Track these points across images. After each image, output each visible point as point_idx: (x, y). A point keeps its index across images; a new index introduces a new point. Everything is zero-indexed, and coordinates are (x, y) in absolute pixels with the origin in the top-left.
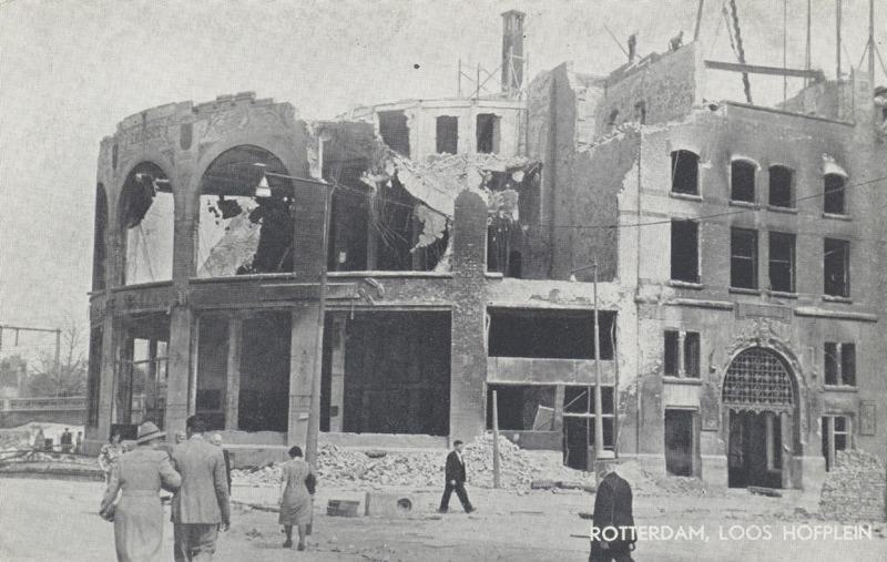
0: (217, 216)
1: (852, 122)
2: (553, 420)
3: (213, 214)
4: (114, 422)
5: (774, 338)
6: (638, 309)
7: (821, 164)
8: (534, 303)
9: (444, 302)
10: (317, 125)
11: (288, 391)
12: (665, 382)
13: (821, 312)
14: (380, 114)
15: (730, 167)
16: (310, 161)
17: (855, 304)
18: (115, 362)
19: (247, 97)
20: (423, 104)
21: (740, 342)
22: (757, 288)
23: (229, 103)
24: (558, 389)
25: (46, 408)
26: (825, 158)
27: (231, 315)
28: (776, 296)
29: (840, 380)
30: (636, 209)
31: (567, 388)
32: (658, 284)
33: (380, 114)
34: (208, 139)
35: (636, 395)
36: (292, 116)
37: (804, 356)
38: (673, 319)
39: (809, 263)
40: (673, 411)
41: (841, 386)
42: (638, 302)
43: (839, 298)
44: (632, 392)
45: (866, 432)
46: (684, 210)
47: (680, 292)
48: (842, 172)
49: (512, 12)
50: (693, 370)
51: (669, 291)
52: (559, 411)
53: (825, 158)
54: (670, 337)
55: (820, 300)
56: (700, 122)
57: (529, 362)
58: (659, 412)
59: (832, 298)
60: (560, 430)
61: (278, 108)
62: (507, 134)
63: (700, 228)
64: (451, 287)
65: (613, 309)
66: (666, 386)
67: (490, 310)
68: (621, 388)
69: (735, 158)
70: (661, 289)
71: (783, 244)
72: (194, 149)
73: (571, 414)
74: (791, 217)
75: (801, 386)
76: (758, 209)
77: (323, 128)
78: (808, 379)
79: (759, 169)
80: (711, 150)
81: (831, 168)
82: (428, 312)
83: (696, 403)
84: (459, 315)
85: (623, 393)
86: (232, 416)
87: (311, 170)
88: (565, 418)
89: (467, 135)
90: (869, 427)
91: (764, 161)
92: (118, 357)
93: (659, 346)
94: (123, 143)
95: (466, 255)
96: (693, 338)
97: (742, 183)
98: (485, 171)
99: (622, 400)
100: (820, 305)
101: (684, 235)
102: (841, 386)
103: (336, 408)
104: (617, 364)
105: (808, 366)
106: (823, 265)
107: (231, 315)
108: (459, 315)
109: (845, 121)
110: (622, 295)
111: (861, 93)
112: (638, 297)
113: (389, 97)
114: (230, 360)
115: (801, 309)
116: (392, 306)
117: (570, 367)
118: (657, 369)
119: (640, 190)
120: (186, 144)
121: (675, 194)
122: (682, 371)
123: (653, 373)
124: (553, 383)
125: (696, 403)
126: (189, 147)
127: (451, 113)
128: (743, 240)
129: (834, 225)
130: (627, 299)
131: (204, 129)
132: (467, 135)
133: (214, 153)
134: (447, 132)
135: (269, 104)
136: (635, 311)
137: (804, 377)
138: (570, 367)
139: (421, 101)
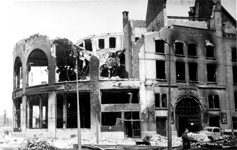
0: (47, 72)
1: (214, 30)
2: (121, 122)
3: (46, 71)
4: (15, 127)
5: (192, 95)
6: (146, 88)
7: (205, 43)
8: (114, 87)
9: (88, 89)
10: (53, 41)
12: (156, 110)
13: (207, 87)
14: (84, 40)
15: (175, 44)
16: (51, 51)
17: (218, 84)
19: (37, 35)
20: (95, 36)
21: (180, 97)
22: (185, 80)
23: (32, 38)
24: (122, 113)
26: (206, 41)
27: (39, 97)
28: (192, 83)
29: (214, 107)
30: (144, 58)
31: (125, 113)
32: (152, 80)
33: (84, 40)
35: (146, 113)
36: (47, 39)
37: (202, 100)
38: (158, 90)
39: (202, 72)
40: (158, 118)
41: (214, 109)
42: (146, 86)
43: (213, 82)
44: (145, 113)
45: (226, 122)
46: (160, 57)
47: (160, 82)
48: (212, 45)
49: (125, 12)
50: (164, 105)
51: (155, 82)
52: (123, 119)
53: (206, 41)
54: (157, 96)
55: (207, 83)
56: (164, 31)
57: (113, 105)
58: (154, 118)
59: (210, 82)
60: (123, 125)
61: (43, 37)
62: (118, 42)
63: (166, 63)
64: (90, 84)
65: (138, 88)
66: (156, 111)
67: (101, 90)
68: (141, 112)
69: (176, 42)
70: (153, 81)
71: (194, 67)
72: (26, 51)
74: (196, 59)
75: (201, 109)
76: (185, 57)
77: (55, 42)
78: (204, 107)
79: (184, 45)
81: (208, 44)
82: (84, 92)
83: (166, 115)
84: (92, 92)
85: (142, 113)
87: (52, 54)
88: (125, 122)
89: (107, 44)
90: (225, 121)
91: (186, 42)
93: (153, 98)
95: (94, 75)
96: (164, 96)
97: (179, 49)
98: (110, 53)
99: (142, 115)
100: (206, 85)
101: (160, 65)
102: (214, 109)
103: (64, 121)
104: (140, 104)
105: (203, 102)
106: (207, 73)
107: (39, 97)
108: (92, 92)
109: (212, 30)
110: (140, 84)
111: (217, 21)
112: (146, 84)
113: (86, 35)
115: (200, 86)
116: (73, 91)
117: (125, 106)
118: (153, 106)
119: (145, 52)
120: (24, 50)
121: (157, 53)
122: (161, 105)
123: (152, 107)
124: (120, 111)
125: (166, 115)
126: (25, 51)
127: (102, 38)
128: (180, 66)
129: (210, 61)
130: (142, 85)
132: (107, 44)
134: (101, 43)
135: (41, 36)
136: (145, 88)
137: (202, 106)
138: (125, 106)
139: (94, 35)
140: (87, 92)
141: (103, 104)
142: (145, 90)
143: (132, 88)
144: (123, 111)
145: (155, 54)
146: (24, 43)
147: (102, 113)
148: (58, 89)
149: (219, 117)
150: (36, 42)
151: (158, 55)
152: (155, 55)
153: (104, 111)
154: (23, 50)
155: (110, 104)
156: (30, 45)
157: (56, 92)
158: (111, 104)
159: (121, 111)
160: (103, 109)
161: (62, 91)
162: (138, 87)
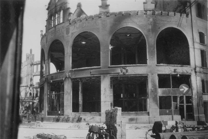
11: (64, 104)
12: (203, 94)
18: (48, 95)
25: (105, 105)
27: (80, 80)
34: (74, 31)
46: (203, 47)
66: (203, 95)
67: (159, 75)
72: (70, 34)
73: (181, 104)
80: (55, 98)
86: (80, 108)
92: (49, 93)
94: (49, 36)
107: (80, 80)
114: (80, 93)
124: (176, 95)
131: (73, 29)
133: (76, 35)
136: (195, 75)
140: (143, 77)
141: (160, 89)
142: (195, 76)
143: (185, 74)
144: (179, 96)
145: (200, 44)
146: (68, 26)
147: (160, 97)
148: (113, 73)
149: (147, 111)
150: (85, 25)
151: (201, 45)
152: (200, 45)
153: (162, 95)
154: (65, 33)
155: (167, 89)
156: (77, 27)
157: (110, 75)
158: (168, 89)
159: (177, 95)
160: (161, 94)
161: (118, 74)
162: (190, 73)
